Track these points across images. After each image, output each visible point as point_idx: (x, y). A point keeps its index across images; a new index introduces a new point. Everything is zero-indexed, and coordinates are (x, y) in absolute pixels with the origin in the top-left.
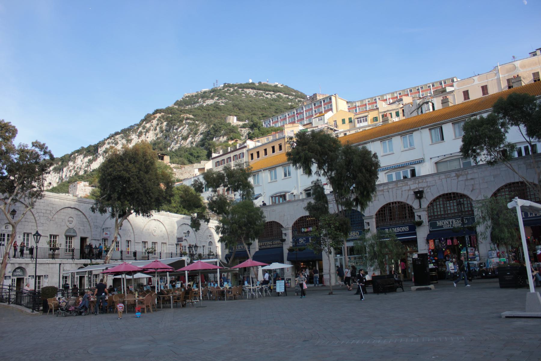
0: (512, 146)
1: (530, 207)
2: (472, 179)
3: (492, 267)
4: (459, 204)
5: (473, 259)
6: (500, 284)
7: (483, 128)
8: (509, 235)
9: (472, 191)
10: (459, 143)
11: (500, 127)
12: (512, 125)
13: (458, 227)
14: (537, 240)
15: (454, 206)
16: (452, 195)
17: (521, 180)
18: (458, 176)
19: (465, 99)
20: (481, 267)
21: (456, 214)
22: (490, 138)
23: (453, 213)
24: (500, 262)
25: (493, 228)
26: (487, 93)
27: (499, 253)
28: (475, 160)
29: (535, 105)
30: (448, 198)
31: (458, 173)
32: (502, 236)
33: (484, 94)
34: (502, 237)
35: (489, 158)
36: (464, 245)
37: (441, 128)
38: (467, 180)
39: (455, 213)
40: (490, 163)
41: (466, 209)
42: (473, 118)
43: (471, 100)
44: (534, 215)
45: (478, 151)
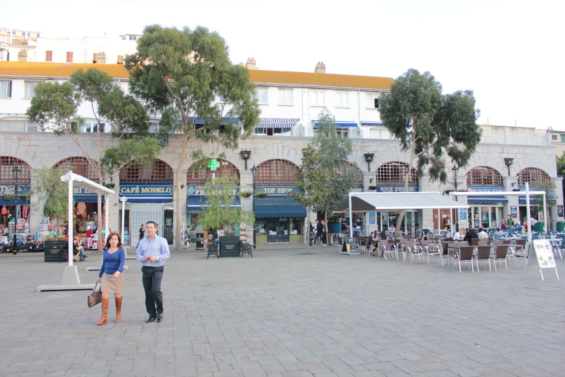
0: (82, 121)
1: (82, 182)
2: (35, 146)
3: (40, 240)
4: (15, 170)
5: (22, 230)
6: (45, 258)
7: (56, 94)
8: (62, 209)
9: (32, 158)
10: (27, 105)
11: (74, 98)
12: (86, 99)
13: (9, 196)
14: (89, 216)
15: (9, 171)
16: (9, 160)
17: (84, 156)
18: (19, 140)
19: (47, 60)
20: (29, 240)
21: (11, 181)
22: (61, 106)
23: (7, 179)
24: (50, 235)
25: (47, 201)
26: (71, 61)
27: (51, 226)
28: (42, 126)
29: (111, 86)
30: (4, 162)
31: (21, 136)
32: (55, 209)
33: (68, 60)
34: (55, 210)
35: (57, 127)
36: (14, 216)
37: (11, 83)
38: (30, 145)
39: (10, 179)
40: (57, 133)
41: (23, 177)
42: (47, 82)
43: (52, 62)
44: (90, 192)
45: (47, 118)
